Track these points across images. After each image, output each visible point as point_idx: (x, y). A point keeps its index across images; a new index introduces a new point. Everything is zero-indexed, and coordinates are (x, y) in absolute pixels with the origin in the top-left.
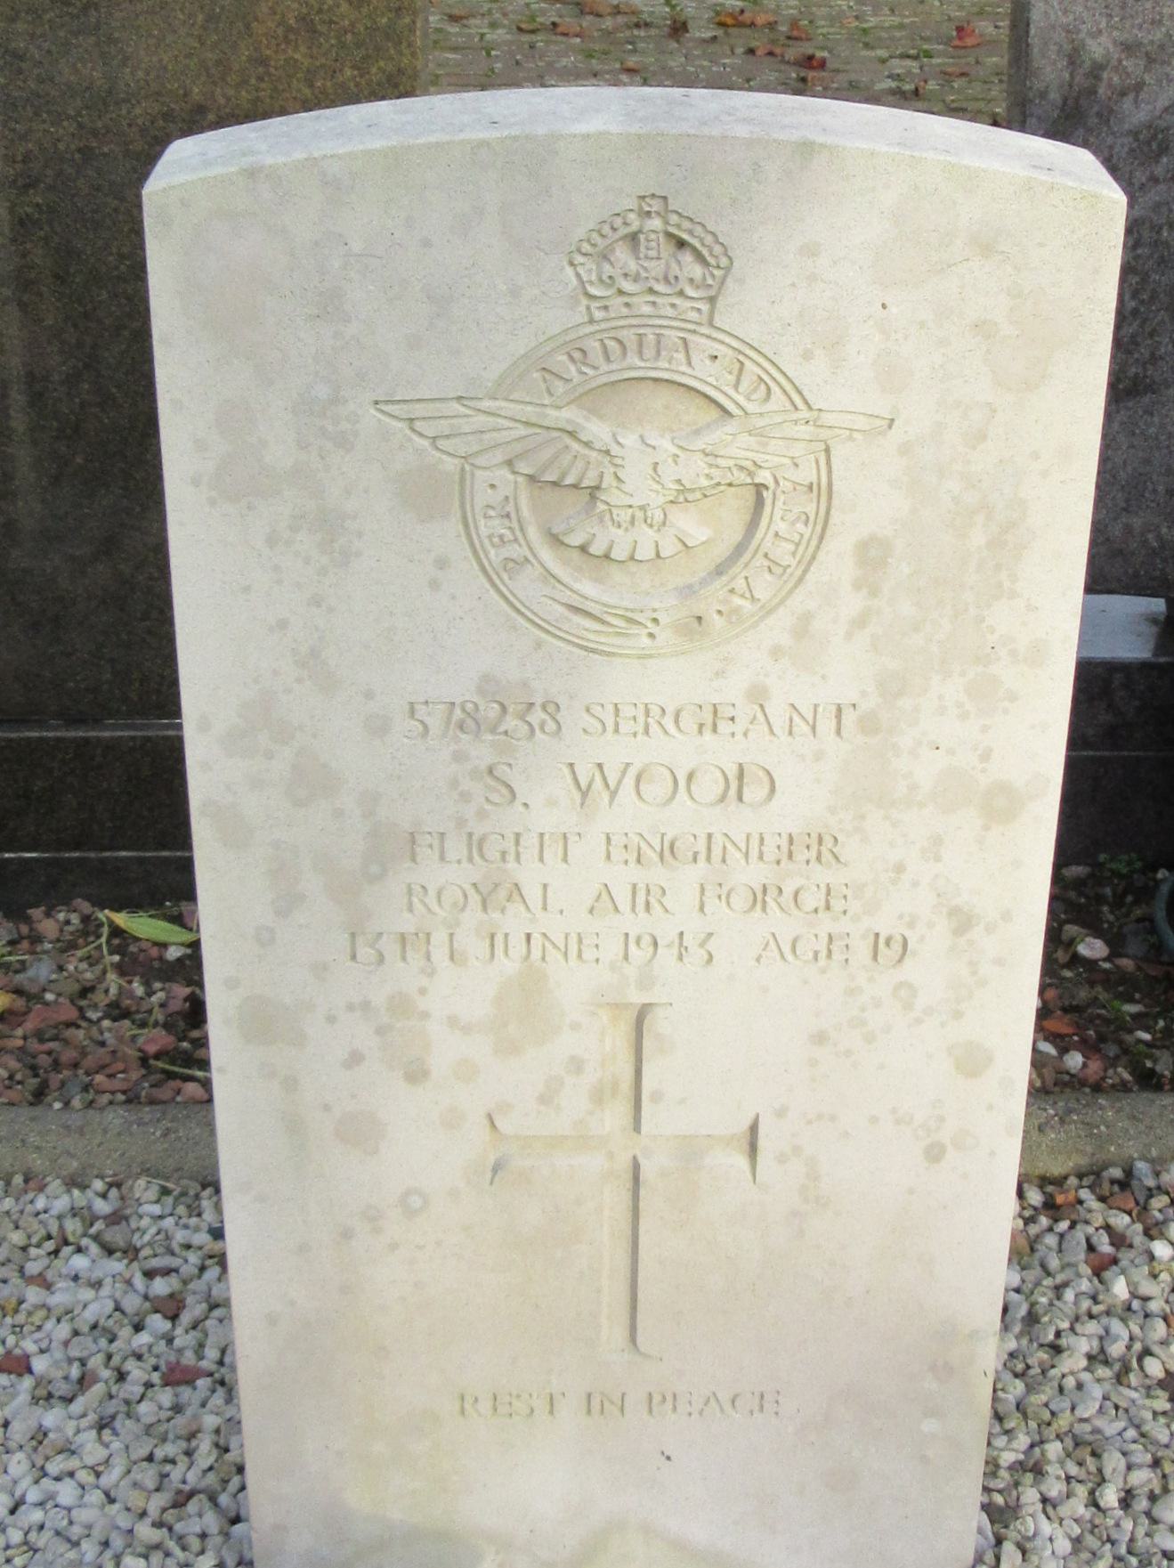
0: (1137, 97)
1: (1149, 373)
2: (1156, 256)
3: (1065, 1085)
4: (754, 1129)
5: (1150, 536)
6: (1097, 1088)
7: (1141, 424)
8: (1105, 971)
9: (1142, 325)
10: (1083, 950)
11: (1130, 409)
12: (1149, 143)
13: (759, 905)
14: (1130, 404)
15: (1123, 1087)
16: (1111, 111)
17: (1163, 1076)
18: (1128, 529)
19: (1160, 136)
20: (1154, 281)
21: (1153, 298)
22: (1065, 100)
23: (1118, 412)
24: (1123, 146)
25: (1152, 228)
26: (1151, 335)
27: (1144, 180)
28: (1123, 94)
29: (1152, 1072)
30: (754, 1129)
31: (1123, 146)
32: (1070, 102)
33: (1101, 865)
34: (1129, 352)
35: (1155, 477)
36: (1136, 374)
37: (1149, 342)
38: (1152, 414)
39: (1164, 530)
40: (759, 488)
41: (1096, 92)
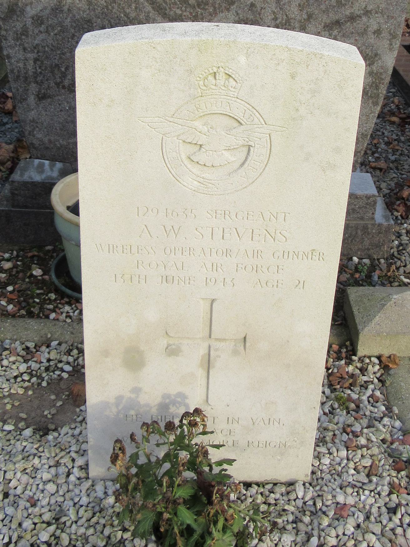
0: (31, 6)
1: (48, 92)
2: (45, 56)
3: (4, 315)
4: (245, 338)
5: (57, 143)
6: (14, 316)
7: (48, 108)
8: (39, 280)
9: (44, 77)
10: (34, 273)
11: (44, 103)
12: (37, 20)
13: (101, 250)
14: (44, 102)
15: (22, 316)
16: (24, 10)
17: (35, 313)
18: (50, 141)
19: (40, 19)
20: (45, 63)
21: (45, 69)
22: (9, 7)
23: (40, 104)
24: (29, 21)
25: (42, 47)
26: (47, 80)
27: (37, 32)
28: (27, 5)
29: (32, 312)
30: (245, 338)
31: (29, 21)
32: (11, 7)
33: (57, 246)
34: (41, 85)
35: (55, 125)
36: (44, 92)
37: (46, 82)
38: (51, 105)
39: (61, 142)
40: (215, 73)
41: (18, 4)
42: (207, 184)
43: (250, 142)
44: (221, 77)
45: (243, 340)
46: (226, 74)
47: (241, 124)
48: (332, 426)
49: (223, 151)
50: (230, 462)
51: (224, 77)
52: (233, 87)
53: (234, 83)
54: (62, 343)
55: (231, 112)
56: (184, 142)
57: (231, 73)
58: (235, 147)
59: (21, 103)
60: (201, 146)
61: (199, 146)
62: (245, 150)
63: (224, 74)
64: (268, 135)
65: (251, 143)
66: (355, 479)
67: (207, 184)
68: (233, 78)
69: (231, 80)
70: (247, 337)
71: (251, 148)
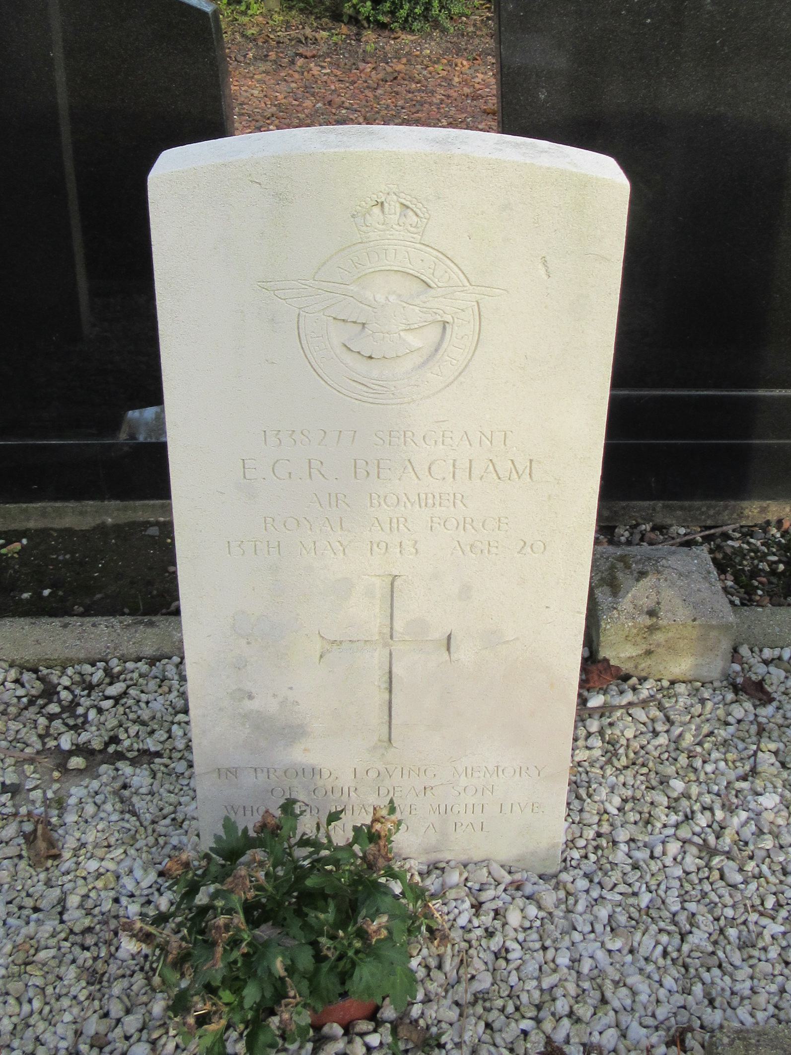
4: (449, 637)
30: (449, 637)
42: (376, 387)
43: (445, 315)
44: (392, 206)
45: (445, 642)
46: (402, 204)
47: (429, 286)
48: (764, 565)
49: (402, 333)
50: (304, 834)
51: (398, 210)
52: (414, 225)
53: (415, 218)
54: (734, 910)
55: (412, 267)
56: (334, 319)
57: (410, 201)
58: (421, 325)
59: (714, 1036)
60: (364, 324)
61: (360, 327)
62: (439, 330)
63: (398, 205)
64: (475, 304)
65: (448, 318)
66: (126, 735)
67: (376, 387)
68: (412, 210)
69: (411, 213)
70: (452, 636)
71: (447, 325)
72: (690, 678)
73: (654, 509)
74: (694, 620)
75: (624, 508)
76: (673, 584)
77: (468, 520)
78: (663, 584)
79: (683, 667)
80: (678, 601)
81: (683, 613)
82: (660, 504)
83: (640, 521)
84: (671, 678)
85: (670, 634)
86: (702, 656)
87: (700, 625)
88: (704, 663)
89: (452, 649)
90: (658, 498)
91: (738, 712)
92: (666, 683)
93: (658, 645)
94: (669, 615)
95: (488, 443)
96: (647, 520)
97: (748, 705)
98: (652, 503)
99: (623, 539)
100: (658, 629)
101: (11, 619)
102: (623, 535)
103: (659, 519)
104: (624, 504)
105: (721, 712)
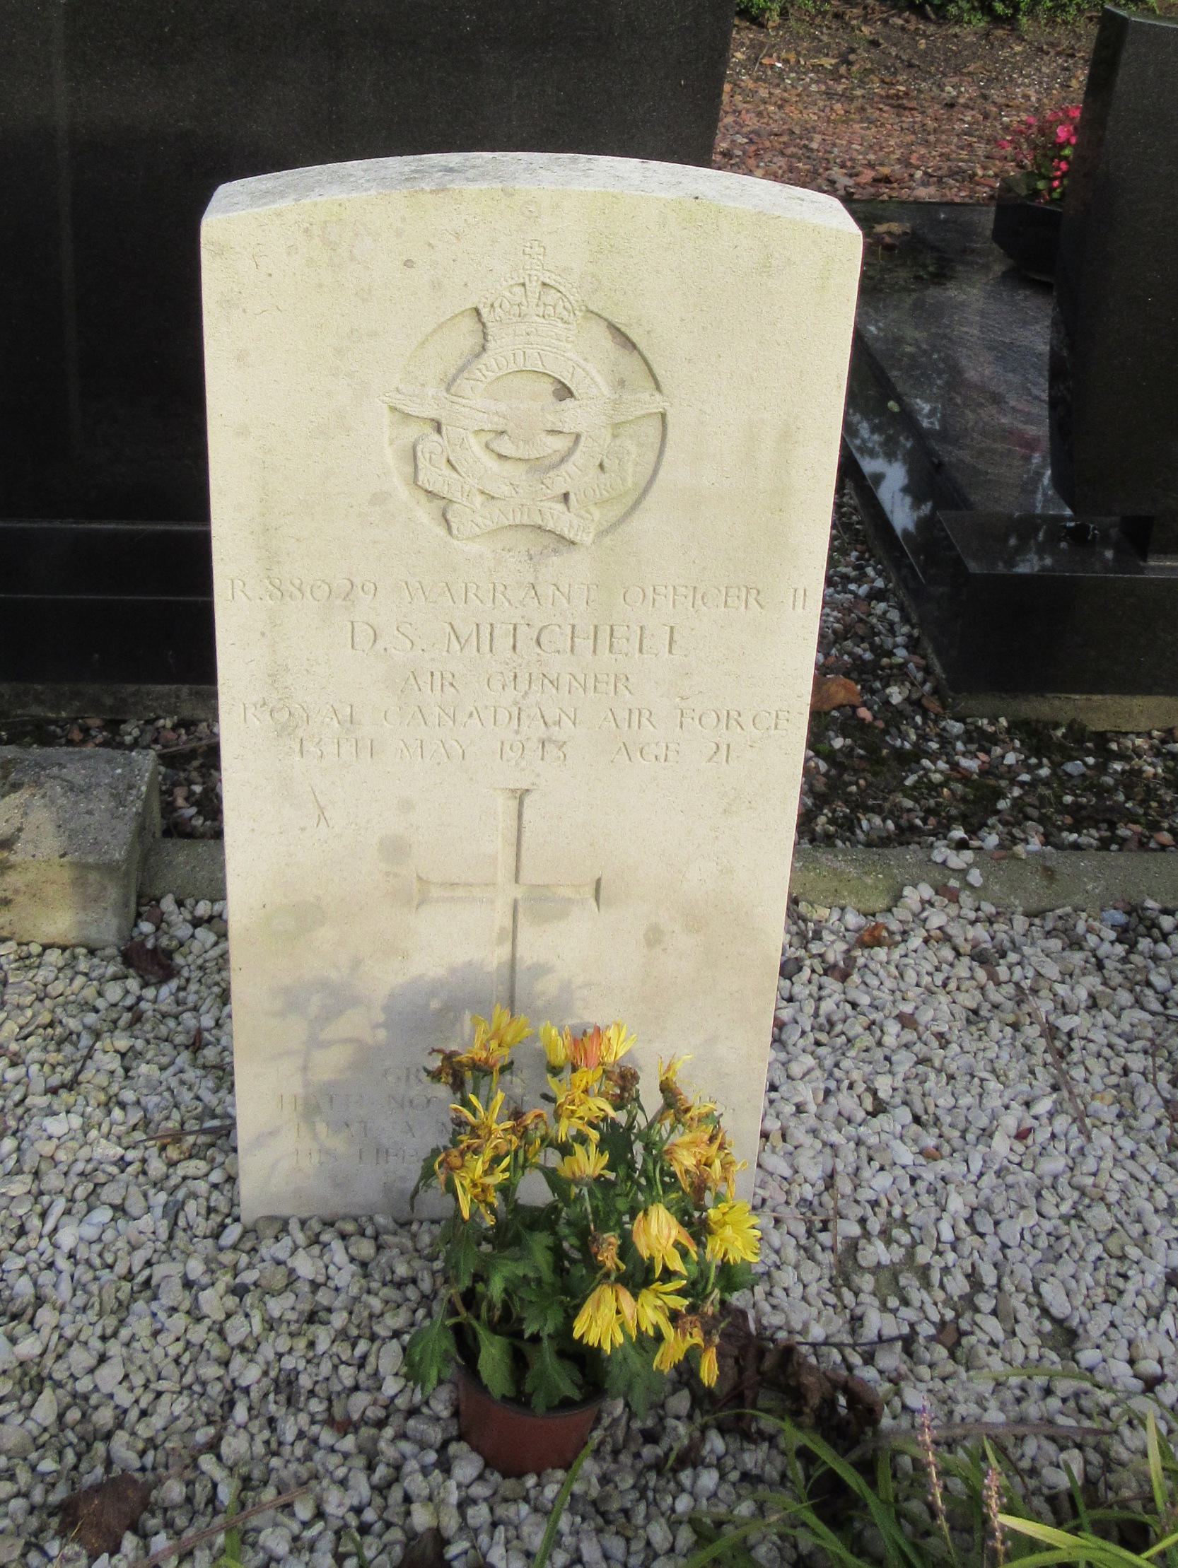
30: (598, 882)
72: (74, 941)
73: (178, 697)
74: (62, 856)
75: (133, 694)
76: (53, 802)
77: (734, 714)
78: (37, 801)
79: (60, 925)
80: (50, 828)
81: (51, 843)
82: (185, 689)
83: (160, 713)
84: (45, 941)
85: (30, 876)
86: (84, 909)
87: (71, 864)
88: (89, 919)
89: (601, 900)
90: (184, 682)
91: (114, 992)
92: (35, 949)
93: (16, 891)
94: (30, 847)
95: (564, 601)
96: (171, 712)
97: (133, 984)
98: (174, 687)
99: (128, 739)
100: (11, 867)
101: (880, 851)
102: (130, 734)
103: (187, 711)
104: (131, 688)
105: (89, 993)
